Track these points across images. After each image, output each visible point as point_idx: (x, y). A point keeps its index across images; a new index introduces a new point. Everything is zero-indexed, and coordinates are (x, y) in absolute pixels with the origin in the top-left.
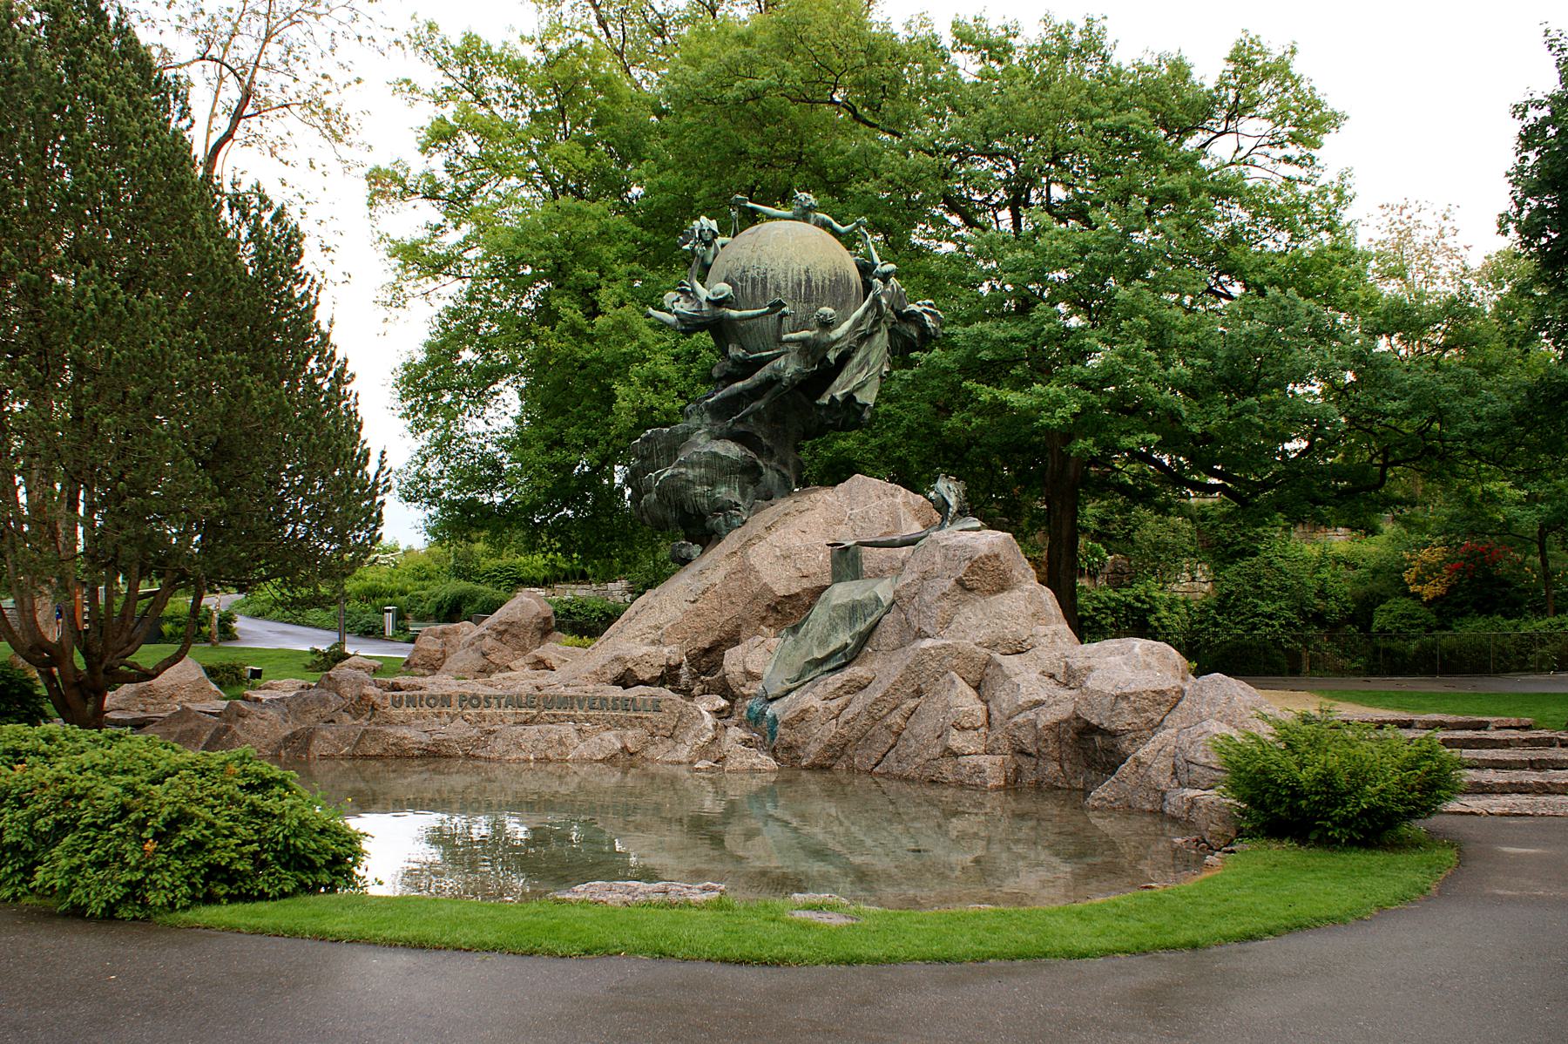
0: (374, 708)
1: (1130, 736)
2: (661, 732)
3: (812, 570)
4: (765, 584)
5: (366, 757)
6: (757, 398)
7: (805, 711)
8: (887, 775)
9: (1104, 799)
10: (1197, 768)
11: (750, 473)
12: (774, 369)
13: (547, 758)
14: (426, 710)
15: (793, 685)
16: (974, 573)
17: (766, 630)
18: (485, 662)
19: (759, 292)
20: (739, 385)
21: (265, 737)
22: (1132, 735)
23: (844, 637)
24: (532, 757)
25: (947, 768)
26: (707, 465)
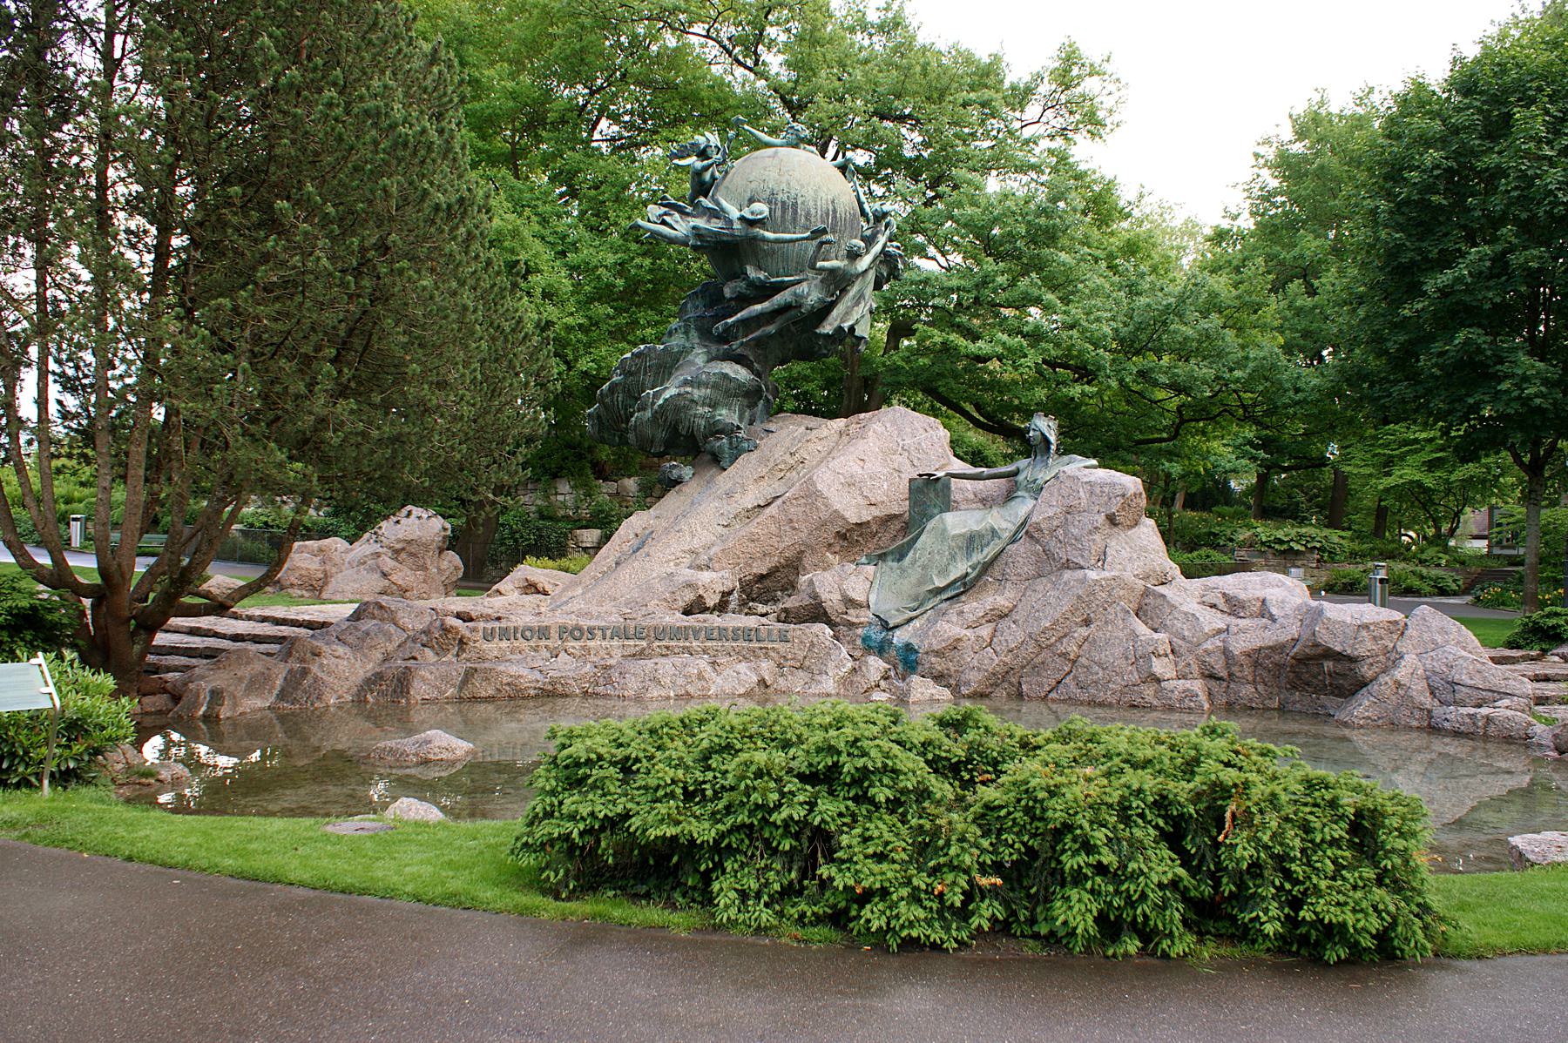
0: (462, 642)
1: (1368, 661)
2: (789, 663)
3: (879, 499)
4: (836, 511)
5: (475, 699)
6: (769, 323)
7: (959, 640)
8: (1053, 700)
9: (1369, 718)
10: (1463, 689)
11: (751, 396)
12: (795, 294)
13: (688, 694)
14: (521, 643)
15: (915, 614)
16: (1124, 509)
17: (831, 556)
18: (386, 582)
19: (789, 216)
20: (758, 307)
21: (347, 679)
22: (1371, 660)
23: (960, 568)
24: (672, 694)
25: (1149, 692)
26: (715, 386)
